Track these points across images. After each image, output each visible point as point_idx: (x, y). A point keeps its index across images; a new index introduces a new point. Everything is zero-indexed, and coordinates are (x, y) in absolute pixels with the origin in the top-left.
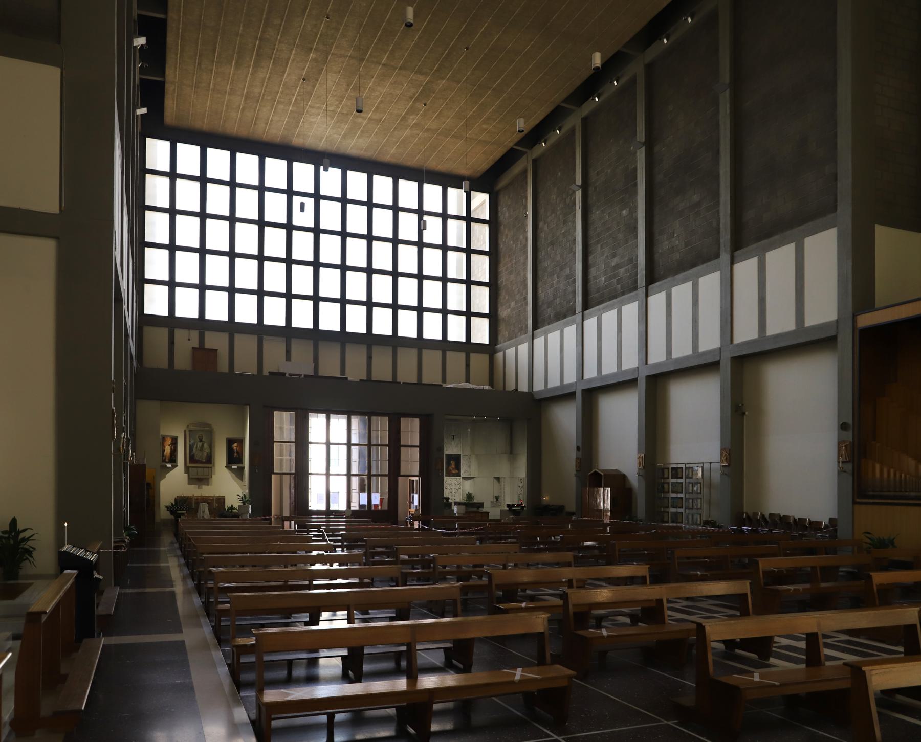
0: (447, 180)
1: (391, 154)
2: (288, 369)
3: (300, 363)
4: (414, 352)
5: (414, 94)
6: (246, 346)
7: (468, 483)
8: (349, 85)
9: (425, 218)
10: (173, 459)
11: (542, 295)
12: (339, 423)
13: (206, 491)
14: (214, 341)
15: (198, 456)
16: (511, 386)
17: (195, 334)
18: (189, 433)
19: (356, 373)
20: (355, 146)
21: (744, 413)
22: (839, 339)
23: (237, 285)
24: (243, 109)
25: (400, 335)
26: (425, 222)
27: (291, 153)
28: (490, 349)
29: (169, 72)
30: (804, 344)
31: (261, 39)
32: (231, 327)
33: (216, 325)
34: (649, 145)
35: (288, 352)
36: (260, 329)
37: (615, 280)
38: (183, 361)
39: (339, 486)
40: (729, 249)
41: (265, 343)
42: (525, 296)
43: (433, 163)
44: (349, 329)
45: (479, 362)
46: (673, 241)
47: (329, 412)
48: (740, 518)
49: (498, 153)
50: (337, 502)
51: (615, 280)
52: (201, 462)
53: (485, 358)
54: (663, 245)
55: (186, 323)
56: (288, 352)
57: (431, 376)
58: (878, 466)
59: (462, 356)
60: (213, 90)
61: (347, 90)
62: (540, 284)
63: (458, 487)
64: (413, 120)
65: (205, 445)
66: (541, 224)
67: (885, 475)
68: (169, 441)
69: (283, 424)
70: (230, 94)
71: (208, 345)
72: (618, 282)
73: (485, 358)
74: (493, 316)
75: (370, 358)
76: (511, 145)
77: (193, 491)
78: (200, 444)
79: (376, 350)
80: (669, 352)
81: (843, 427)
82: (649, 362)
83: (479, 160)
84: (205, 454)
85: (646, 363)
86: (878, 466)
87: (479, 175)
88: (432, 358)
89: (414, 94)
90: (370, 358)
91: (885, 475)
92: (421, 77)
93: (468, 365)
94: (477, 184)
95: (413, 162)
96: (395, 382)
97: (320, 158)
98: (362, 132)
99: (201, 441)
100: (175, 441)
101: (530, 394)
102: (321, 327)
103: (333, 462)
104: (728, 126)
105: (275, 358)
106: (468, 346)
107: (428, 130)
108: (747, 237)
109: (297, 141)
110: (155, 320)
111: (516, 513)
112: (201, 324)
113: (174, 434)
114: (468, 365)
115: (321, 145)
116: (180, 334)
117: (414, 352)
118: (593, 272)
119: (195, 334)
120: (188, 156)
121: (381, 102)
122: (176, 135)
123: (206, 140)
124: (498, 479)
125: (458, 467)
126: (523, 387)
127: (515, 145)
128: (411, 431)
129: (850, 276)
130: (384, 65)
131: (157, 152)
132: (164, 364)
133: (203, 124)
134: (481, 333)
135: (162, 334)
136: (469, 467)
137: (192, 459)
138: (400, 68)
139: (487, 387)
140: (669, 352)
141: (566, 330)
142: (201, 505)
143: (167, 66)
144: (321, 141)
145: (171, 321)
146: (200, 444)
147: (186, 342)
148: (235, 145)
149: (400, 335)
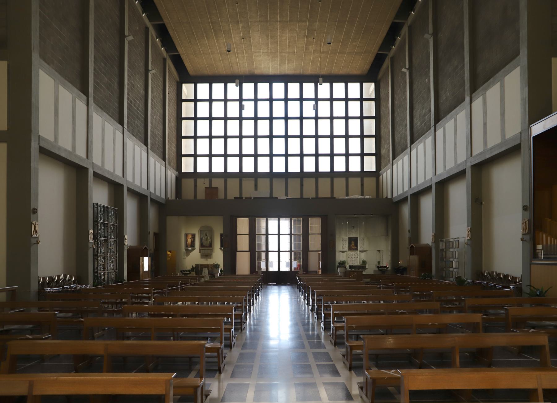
0: (346, 79)
1: (310, 70)
2: (254, 194)
3: (263, 191)
4: (313, 180)
5: (305, 34)
6: (233, 184)
7: (363, 254)
8: (267, 37)
9: (244, 103)
10: (193, 245)
11: (396, 138)
12: (285, 223)
13: (210, 262)
14: (218, 183)
15: (205, 243)
16: (385, 196)
17: (207, 180)
18: (201, 232)
19: (294, 193)
20: (288, 69)
21: (482, 203)
22: (522, 146)
23: (274, 153)
24: (223, 60)
25: (335, 171)
26: (244, 105)
27: (255, 79)
28: (376, 175)
29: (179, 49)
30: (512, 151)
31: (212, 23)
32: (226, 175)
33: (218, 175)
34: (435, 35)
35: (256, 186)
36: (241, 175)
37: (423, 124)
38: (201, 195)
39: (285, 257)
40: (469, 93)
41: (243, 182)
42: (391, 142)
43: (335, 71)
44: (290, 170)
45: (369, 182)
46: (446, 95)
47: (279, 217)
48: (479, 274)
49: (371, 58)
50: (272, 267)
51: (423, 124)
52: (207, 247)
53: (374, 179)
54: (443, 98)
55: (203, 175)
56: (256, 186)
57: (340, 194)
58: (544, 236)
59: (359, 180)
60: (203, 53)
61: (268, 39)
62: (396, 132)
63: (356, 256)
64: (312, 48)
65: (209, 238)
66: (395, 96)
67: (553, 243)
68: (190, 236)
69: (243, 225)
70: (212, 54)
71: (214, 186)
72: (425, 125)
73: (374, 179)
74: (378, 155)
75: (302, 185)
76: (376, 51)
77: (204, 262)
78: (206, 237)
79: (275, 181)
80: (445, 167)
81: (525, 208)
82: (437, 174)
83: (361, 65)
84: (208, 242)
85: (435, 175)
86: (544, 236)
87: (366, 72)
88: (340, 183)
89: (305, 34)
90: (302, 185)
91: (553, 243)
92: (304, 24)
93: (362, 185)
94: (361, 79)
95: (324, 72)
96: (332, 198)
97: (270, 79)
98: (288, 60)
99: (206, 235)
100: (193, 236)
101: (391, 199)
102: (350, 170)
103: (279, 242)
104: (467, 11)
105: (249, 191)
106: (363, 174)
107: (323, 52)
108: (478, 83)
109: (257, 72)
110: (188, 175)
111: (383, 272)
112: (210, 175)
113: (193, 232)
114: (362, 185)
115: (271, 72)
116: (200, 181)
117: (313, 180)
118: (415, 120)
119: (207, 180)
120: (203, 89)
121: (289, 42)
122: (196, 80)
123: (211, 80)
124: (379, 251)
125: (356, 245)
126: (389, 197)
127: (379, 50)
128: (315, 225)
129: (527, 99)
130: (280, 21)
131: (187, 90)
132: (192, 197)
133: (208, 72)
134: (370, 165)
135: (191, 181)
136: (364, 244)
137: (202, 245)
138: (289, 21)
139: (360, 197)
140: (445, 167)
141: (404, 158)
142: (204, 269)
143: (177, 46)
144: (269, 69)
145: (195, 175)
146: (206, 237)
147: (202, 184)
148: (226, 79)
149: (335, 171)
